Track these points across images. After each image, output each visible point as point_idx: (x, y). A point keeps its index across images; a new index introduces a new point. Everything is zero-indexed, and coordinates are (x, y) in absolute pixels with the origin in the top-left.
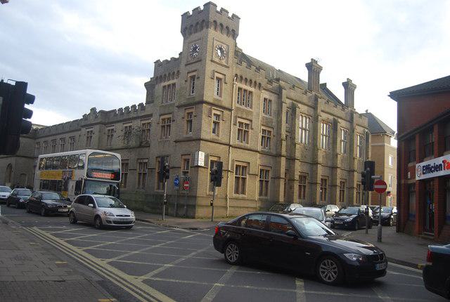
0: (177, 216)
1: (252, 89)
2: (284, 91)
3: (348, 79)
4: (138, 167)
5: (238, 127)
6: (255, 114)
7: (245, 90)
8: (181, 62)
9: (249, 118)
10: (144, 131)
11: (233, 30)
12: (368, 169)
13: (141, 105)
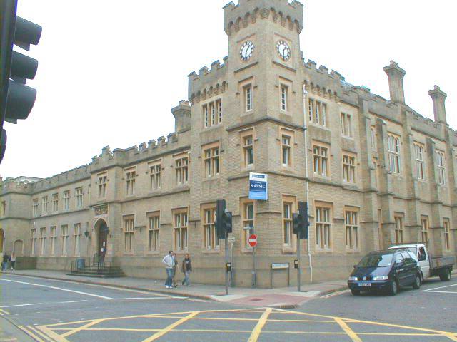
1: (326, 101)
2: (365, 103)
6: (333, 134)
8: (226, 70)
11: (296, 21)
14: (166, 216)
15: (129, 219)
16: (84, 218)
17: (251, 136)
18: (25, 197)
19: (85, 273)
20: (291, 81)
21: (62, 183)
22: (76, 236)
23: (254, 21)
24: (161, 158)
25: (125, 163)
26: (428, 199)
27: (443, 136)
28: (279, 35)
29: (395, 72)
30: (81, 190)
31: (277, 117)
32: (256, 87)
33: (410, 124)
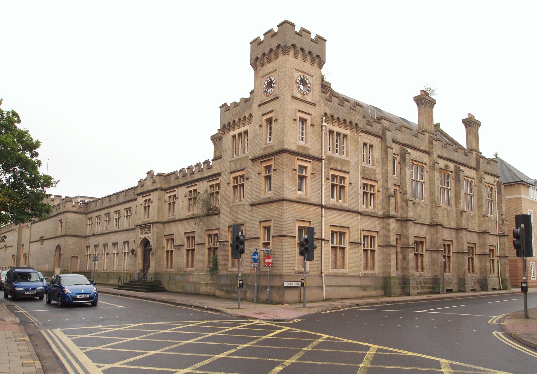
0: (258, 301)
1: (347, 132)
2: (388, 133)
3: (469, 114)
4: (207, 241)
5: (330, 182)
6: (352, 163)
7: (338, 134)
8: (252, 103)
9: (345, 169)
10: (212, 194)
11: (318, 56)
12: (523, 226)
13: (207, 162)
14: (179, 239)
15: (170, 239)
16: (130, 236)
17: (270, 166)
18: (79, 216)
19: (141, 288)
20: (310, 115)
21: (113, 203)
22: (125, 253)
23: (277, 57)
24: (198, 183)
25: (167, 186)
26: (453, 225)
27: (473, 164)
28: (299, 71)
29: (424, 102)
30: (130, 210)
31: (294, 148)
32: (276, 120)
33: (438, 150)
